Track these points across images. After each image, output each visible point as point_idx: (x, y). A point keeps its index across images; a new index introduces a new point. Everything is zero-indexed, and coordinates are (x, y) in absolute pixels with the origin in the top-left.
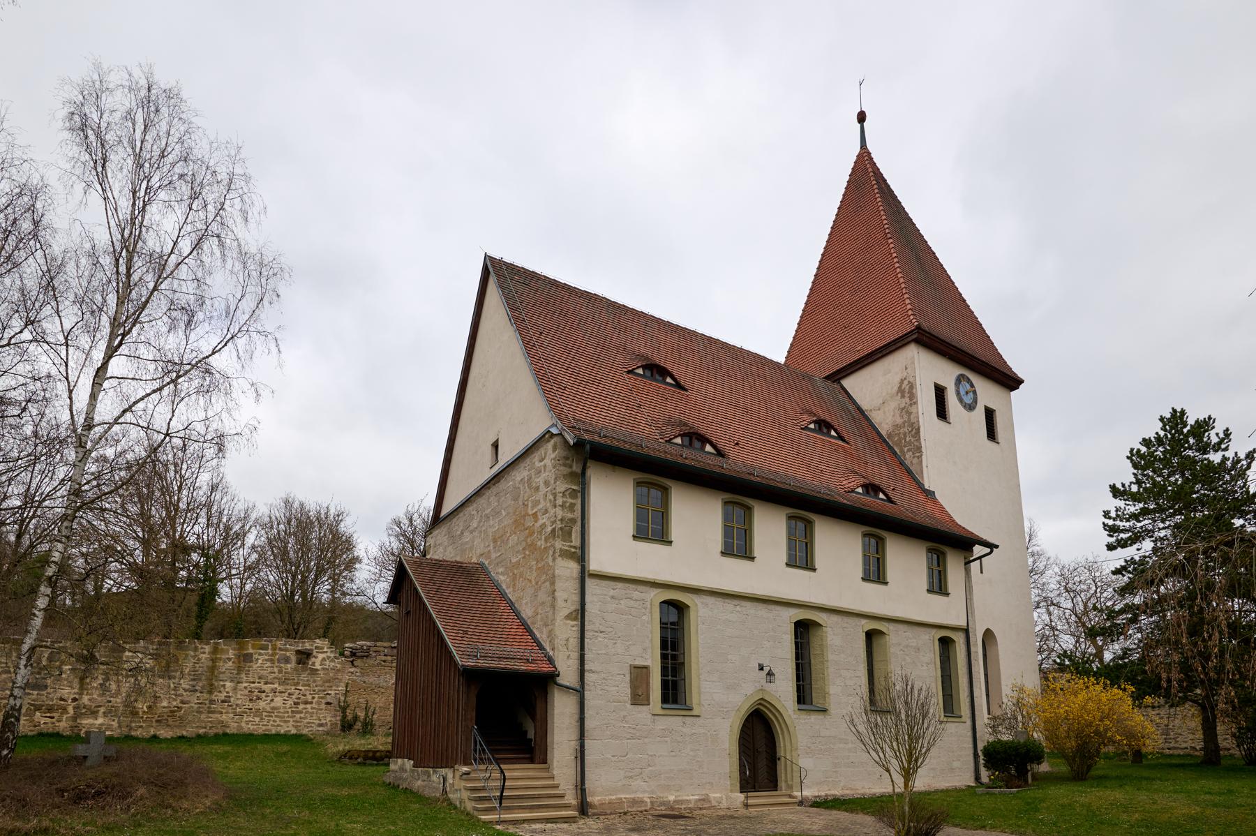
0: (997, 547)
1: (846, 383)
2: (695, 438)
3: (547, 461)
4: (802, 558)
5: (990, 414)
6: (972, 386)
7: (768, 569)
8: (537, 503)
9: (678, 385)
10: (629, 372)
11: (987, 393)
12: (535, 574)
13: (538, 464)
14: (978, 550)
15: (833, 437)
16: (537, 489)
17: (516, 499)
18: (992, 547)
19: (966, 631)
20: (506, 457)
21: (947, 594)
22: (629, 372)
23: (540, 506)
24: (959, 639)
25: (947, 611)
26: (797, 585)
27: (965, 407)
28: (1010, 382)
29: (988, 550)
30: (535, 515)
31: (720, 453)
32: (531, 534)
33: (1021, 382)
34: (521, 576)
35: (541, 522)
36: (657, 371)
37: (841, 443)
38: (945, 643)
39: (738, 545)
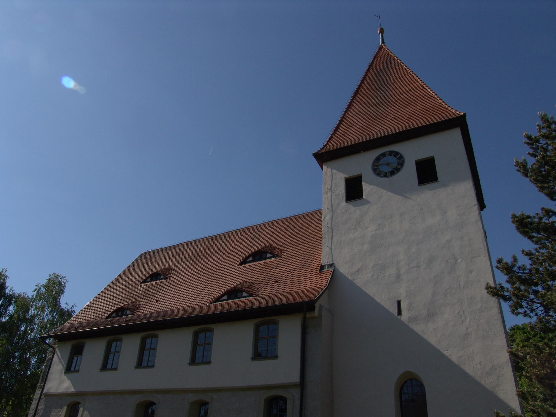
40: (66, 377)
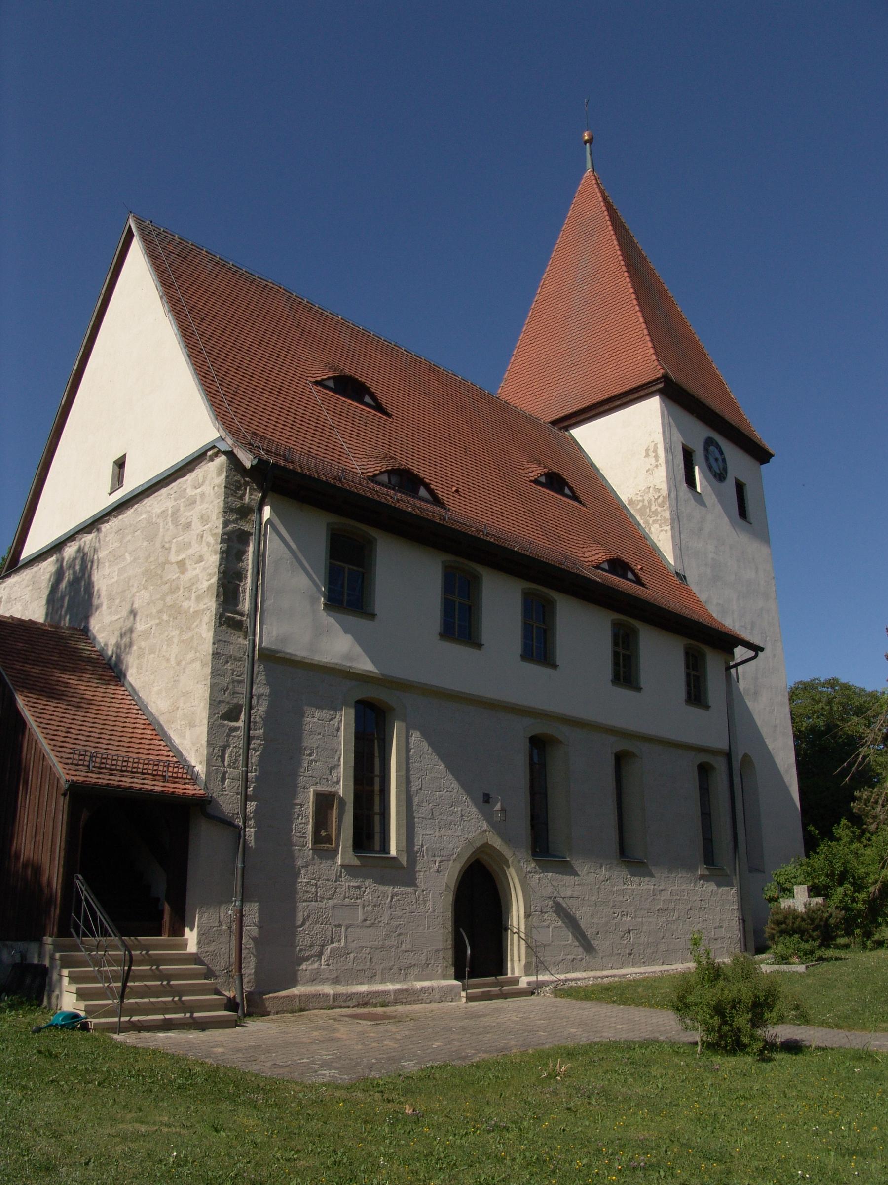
0: (762, 649)
1: (579, 433)
2: (407, 480)
3: (207, 489)
4: (539, 647)
5: (740, 488)
6: (721, 453)
7: (495, 666)
8: (187, 545)
9: (379, 407)
10: (317, 383)
11: (737, 462)
12: (175, 649)
13: (190, 492)
14: (740, 653)
15: (422, 499)
16: (188, 526)
17: (151, 539)
18: (758, 650)
19: (728, 756)
20: (133, 481)
21: (554, 666)
22: (317, 383)
23: (190, 552)
24: (720, 765)
25: (704, 728)
26: (531, 686)
27: (715, 476)
28: (762, 455)
29: (752, 654)
30: (181, 565)
31: (436, 500)
32: (173, 591)
33: (771, 455)
34: (152, 651)
35: (190, 574)
36: (349, 387)
37: (576, 504)
38: (704, 770)
39: (460, 623)
40: (332, 620)
